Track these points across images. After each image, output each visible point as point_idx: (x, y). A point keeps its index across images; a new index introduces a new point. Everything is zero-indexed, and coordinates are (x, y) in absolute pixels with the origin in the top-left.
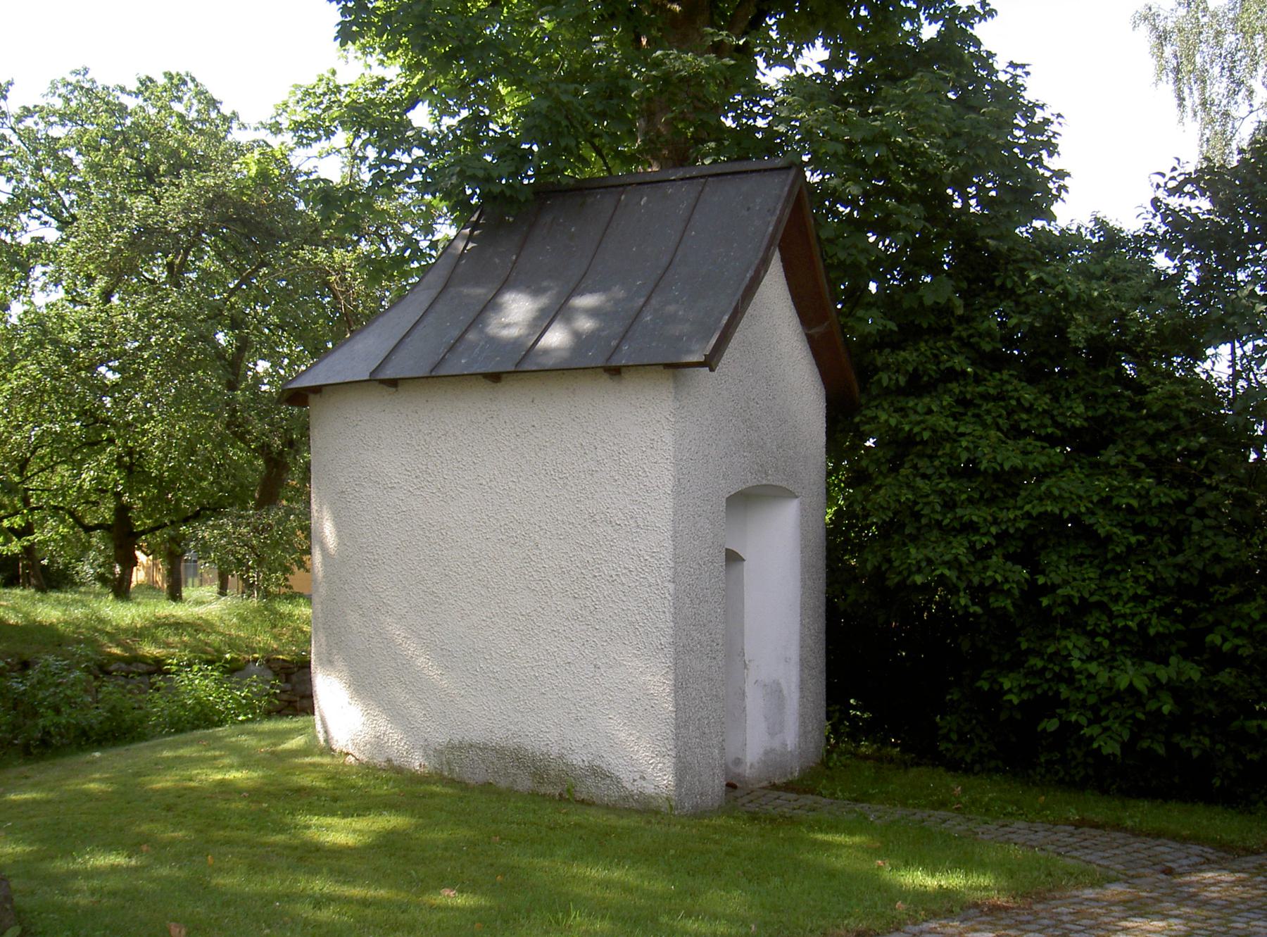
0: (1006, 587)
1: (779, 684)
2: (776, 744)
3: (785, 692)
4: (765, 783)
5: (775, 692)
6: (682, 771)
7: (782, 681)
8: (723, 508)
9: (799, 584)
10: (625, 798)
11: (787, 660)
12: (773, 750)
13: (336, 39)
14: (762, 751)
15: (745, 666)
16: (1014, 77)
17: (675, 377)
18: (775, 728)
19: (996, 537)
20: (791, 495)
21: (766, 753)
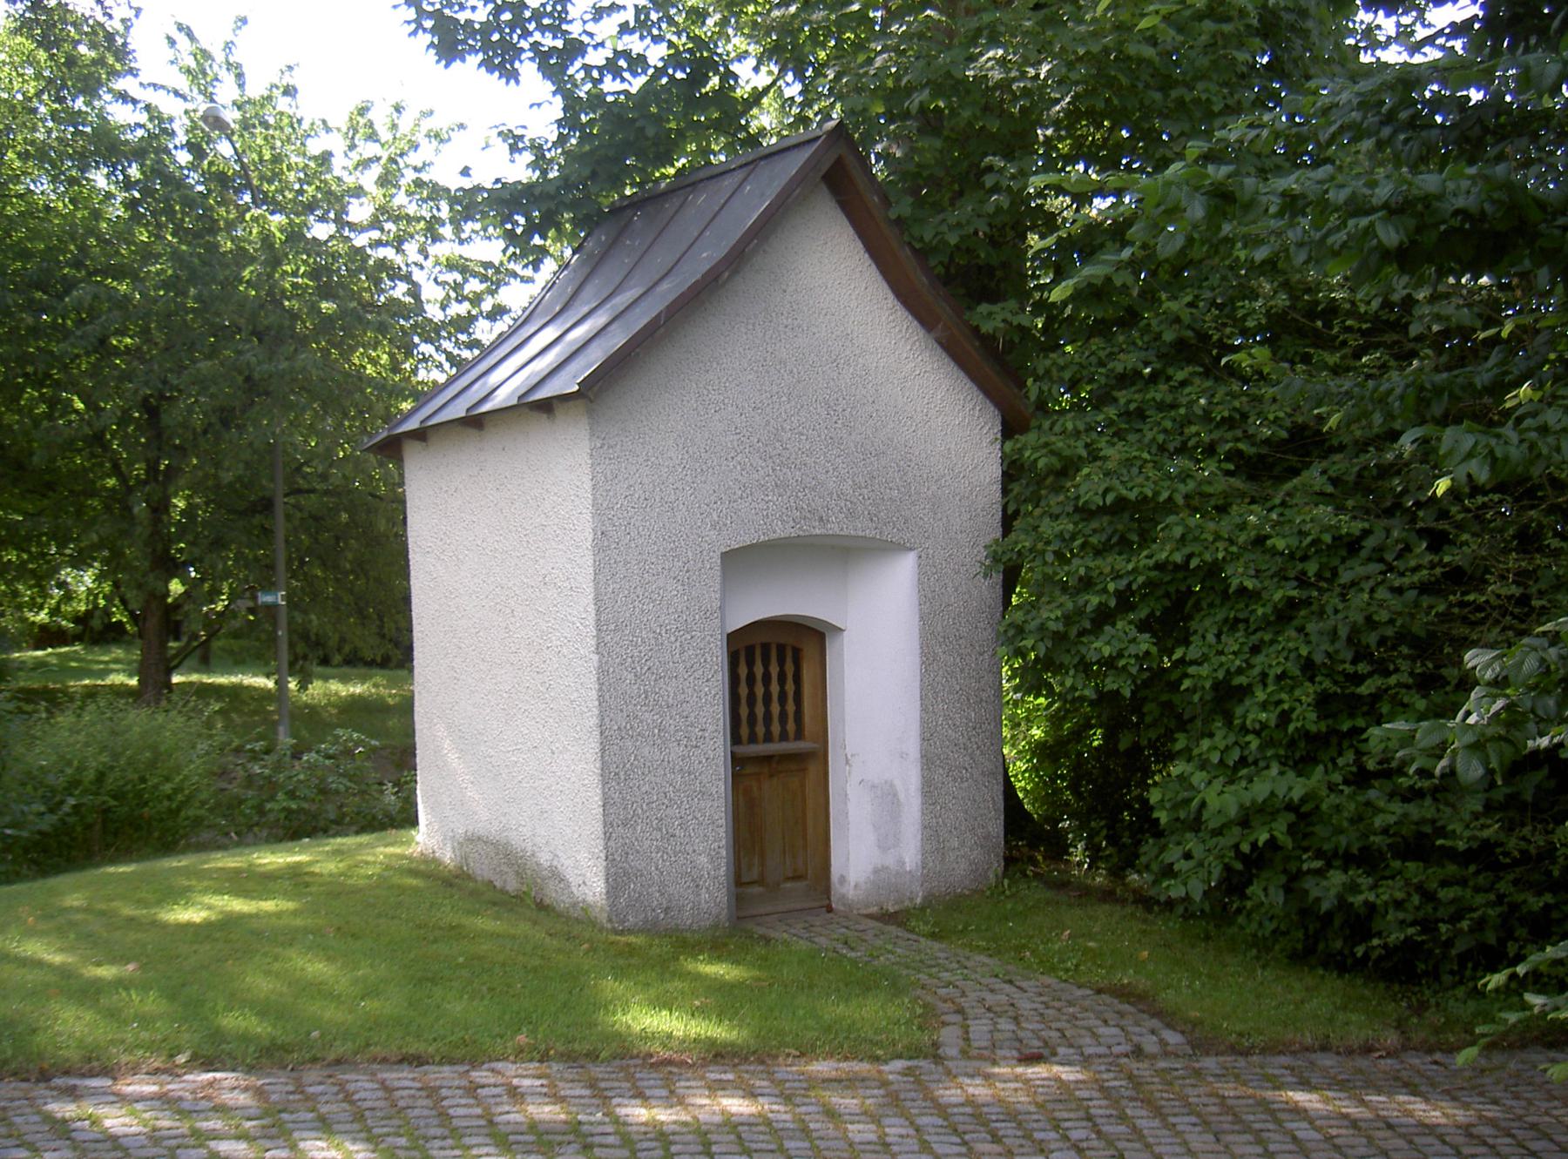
0: (1122, 663)
1: (892, 785)
2: (890, 861)
3: (902, 796)
4: (874, 910)
5: (888, 797)
6: (617, 880)
7: (897, 783)
8: (717, 571)
9: (918, 660)
10: (575, 905)
11: (903, 756)
12: (885, 868)
13: (438, 62)
14: (870, 868)
15: (847, 762)
16: (100, 61)
17: (591, 413)
18: (887, 841)
19: (1119, 594)
20: (901, 548)
21: (876, 871)
